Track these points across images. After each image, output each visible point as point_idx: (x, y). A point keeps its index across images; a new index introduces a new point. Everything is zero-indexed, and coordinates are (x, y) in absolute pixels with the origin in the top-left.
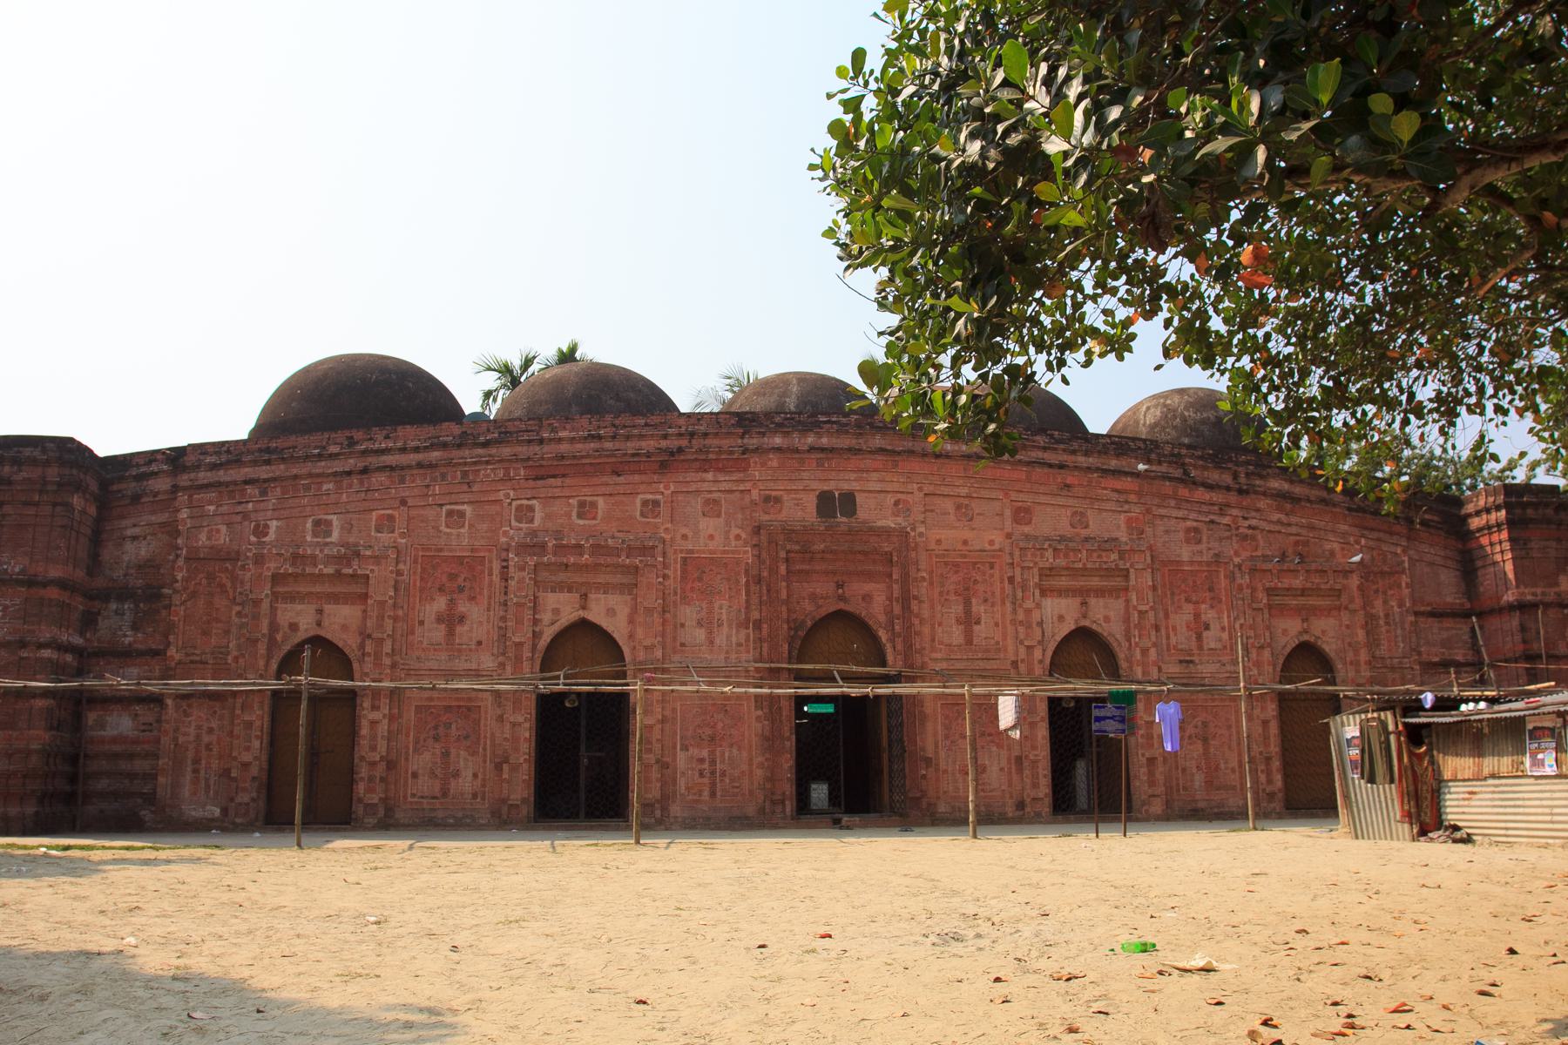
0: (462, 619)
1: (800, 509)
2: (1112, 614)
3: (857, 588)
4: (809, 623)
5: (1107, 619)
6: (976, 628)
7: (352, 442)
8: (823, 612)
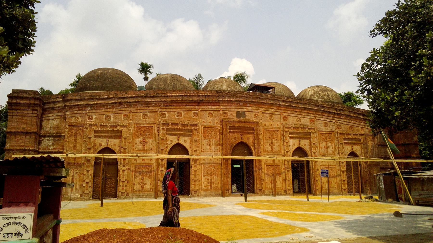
0: (147, 143)
1: (232, 116)
2: (306, 144)
3: (245, 136)
4: (235, 145)
5: (305, 145)
6: (274, 146)
7: (117, 95)
8: (238, 142)
